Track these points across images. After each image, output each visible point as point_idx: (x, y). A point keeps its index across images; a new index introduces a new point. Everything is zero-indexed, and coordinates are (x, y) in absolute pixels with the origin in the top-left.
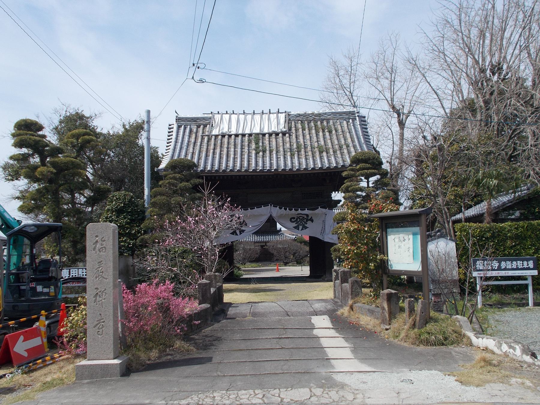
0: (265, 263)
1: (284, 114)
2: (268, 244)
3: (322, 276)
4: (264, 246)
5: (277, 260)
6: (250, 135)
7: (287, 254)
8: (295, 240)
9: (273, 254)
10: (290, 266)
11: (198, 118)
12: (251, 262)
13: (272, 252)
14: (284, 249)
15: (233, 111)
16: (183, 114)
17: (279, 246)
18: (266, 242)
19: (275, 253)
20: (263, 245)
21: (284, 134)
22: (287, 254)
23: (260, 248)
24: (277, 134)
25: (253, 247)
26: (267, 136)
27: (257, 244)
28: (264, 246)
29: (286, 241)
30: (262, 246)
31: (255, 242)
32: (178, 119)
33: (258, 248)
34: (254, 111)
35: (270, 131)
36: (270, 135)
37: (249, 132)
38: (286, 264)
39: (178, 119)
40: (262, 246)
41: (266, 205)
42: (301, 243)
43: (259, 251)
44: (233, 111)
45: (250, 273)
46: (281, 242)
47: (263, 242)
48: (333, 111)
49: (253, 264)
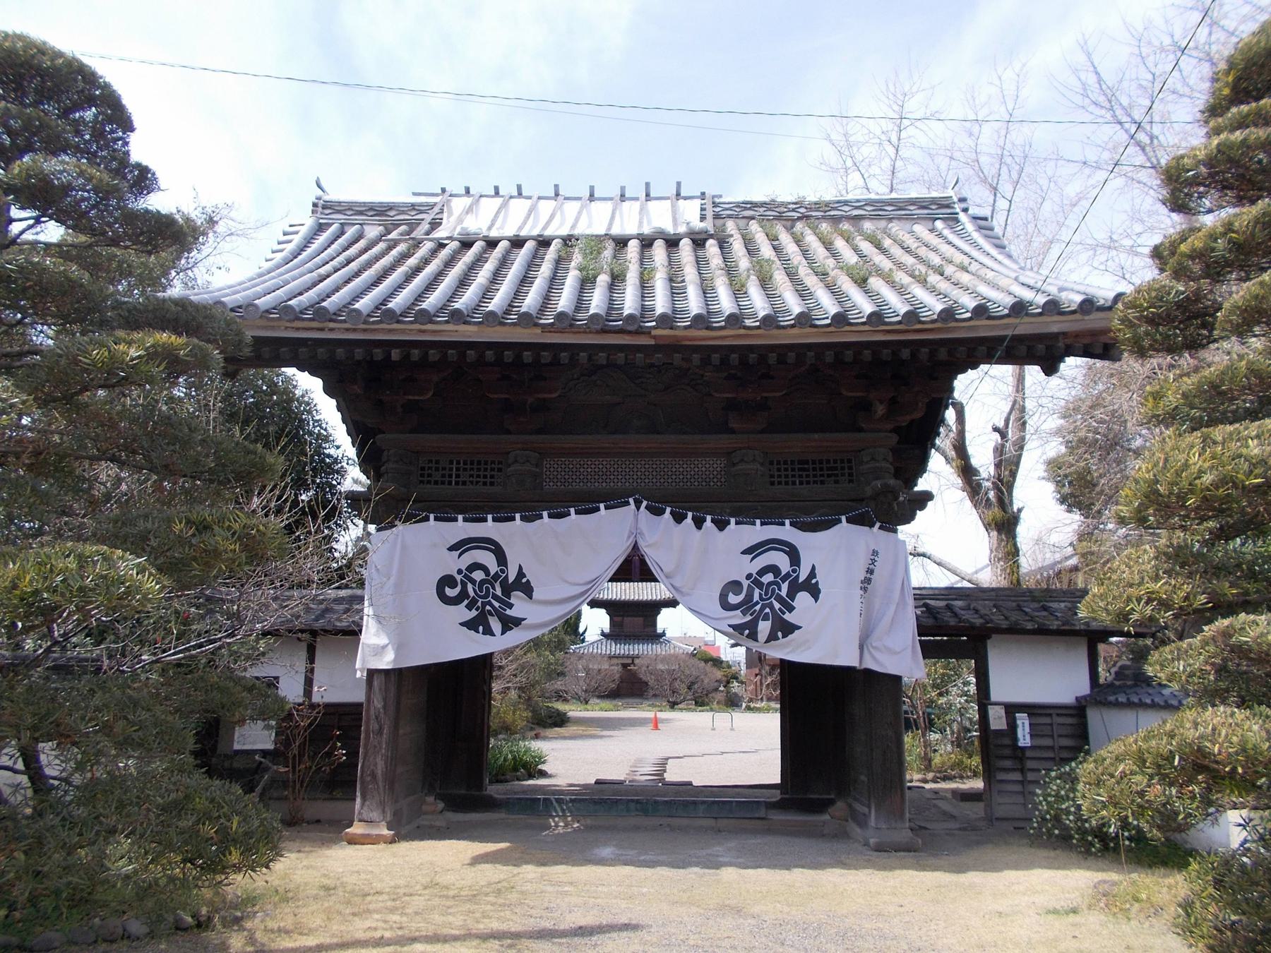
0: (630, 700)
1: (698, 202)
2: (637, 661)
3: (831, 802)
4: (629, 665)
5: (655, 696)
6: (568, 241)
7: (676, 684)
8: (693, 655)
9: (646, 684)
10: (681, 710)
11: (391, 207)
12: (599, 697)
13: (644, 679)
14: (671, 672)
15: (519, 187)
16: (338, 193)
17: (660, 667)
18: (633, 658)
19: (651, 683)
20: (627, 664)
21: (699, 242)
22: (676, 684)
23: (620, 668)
24: (672, 243)
25: (605, 666)
26: (633, 246)
27: (615, 661)
28: (629, 665)
29: (676, 656)
30: (625, 666)
31: (611, 657)
32: (323, 207)
33: (617, 670)
34: (592, 189)
35: (647, 230)
36: (647, 243)
37: (564, 232)
38: (673, 705)
39: (323, 207)
40: (625, 666)
41: (615, 500)
42: (706, 661)
43: (617, 676)
44: (519, 187)
45: (592, 731)
46: (665, 659)
47: (628, 657)
48: (873, 196)
49: (606, 704)
